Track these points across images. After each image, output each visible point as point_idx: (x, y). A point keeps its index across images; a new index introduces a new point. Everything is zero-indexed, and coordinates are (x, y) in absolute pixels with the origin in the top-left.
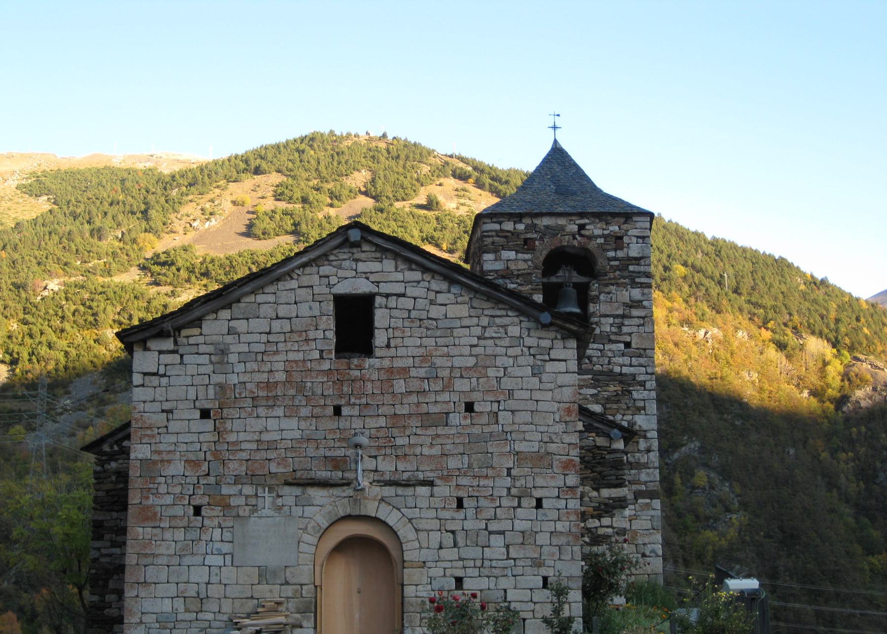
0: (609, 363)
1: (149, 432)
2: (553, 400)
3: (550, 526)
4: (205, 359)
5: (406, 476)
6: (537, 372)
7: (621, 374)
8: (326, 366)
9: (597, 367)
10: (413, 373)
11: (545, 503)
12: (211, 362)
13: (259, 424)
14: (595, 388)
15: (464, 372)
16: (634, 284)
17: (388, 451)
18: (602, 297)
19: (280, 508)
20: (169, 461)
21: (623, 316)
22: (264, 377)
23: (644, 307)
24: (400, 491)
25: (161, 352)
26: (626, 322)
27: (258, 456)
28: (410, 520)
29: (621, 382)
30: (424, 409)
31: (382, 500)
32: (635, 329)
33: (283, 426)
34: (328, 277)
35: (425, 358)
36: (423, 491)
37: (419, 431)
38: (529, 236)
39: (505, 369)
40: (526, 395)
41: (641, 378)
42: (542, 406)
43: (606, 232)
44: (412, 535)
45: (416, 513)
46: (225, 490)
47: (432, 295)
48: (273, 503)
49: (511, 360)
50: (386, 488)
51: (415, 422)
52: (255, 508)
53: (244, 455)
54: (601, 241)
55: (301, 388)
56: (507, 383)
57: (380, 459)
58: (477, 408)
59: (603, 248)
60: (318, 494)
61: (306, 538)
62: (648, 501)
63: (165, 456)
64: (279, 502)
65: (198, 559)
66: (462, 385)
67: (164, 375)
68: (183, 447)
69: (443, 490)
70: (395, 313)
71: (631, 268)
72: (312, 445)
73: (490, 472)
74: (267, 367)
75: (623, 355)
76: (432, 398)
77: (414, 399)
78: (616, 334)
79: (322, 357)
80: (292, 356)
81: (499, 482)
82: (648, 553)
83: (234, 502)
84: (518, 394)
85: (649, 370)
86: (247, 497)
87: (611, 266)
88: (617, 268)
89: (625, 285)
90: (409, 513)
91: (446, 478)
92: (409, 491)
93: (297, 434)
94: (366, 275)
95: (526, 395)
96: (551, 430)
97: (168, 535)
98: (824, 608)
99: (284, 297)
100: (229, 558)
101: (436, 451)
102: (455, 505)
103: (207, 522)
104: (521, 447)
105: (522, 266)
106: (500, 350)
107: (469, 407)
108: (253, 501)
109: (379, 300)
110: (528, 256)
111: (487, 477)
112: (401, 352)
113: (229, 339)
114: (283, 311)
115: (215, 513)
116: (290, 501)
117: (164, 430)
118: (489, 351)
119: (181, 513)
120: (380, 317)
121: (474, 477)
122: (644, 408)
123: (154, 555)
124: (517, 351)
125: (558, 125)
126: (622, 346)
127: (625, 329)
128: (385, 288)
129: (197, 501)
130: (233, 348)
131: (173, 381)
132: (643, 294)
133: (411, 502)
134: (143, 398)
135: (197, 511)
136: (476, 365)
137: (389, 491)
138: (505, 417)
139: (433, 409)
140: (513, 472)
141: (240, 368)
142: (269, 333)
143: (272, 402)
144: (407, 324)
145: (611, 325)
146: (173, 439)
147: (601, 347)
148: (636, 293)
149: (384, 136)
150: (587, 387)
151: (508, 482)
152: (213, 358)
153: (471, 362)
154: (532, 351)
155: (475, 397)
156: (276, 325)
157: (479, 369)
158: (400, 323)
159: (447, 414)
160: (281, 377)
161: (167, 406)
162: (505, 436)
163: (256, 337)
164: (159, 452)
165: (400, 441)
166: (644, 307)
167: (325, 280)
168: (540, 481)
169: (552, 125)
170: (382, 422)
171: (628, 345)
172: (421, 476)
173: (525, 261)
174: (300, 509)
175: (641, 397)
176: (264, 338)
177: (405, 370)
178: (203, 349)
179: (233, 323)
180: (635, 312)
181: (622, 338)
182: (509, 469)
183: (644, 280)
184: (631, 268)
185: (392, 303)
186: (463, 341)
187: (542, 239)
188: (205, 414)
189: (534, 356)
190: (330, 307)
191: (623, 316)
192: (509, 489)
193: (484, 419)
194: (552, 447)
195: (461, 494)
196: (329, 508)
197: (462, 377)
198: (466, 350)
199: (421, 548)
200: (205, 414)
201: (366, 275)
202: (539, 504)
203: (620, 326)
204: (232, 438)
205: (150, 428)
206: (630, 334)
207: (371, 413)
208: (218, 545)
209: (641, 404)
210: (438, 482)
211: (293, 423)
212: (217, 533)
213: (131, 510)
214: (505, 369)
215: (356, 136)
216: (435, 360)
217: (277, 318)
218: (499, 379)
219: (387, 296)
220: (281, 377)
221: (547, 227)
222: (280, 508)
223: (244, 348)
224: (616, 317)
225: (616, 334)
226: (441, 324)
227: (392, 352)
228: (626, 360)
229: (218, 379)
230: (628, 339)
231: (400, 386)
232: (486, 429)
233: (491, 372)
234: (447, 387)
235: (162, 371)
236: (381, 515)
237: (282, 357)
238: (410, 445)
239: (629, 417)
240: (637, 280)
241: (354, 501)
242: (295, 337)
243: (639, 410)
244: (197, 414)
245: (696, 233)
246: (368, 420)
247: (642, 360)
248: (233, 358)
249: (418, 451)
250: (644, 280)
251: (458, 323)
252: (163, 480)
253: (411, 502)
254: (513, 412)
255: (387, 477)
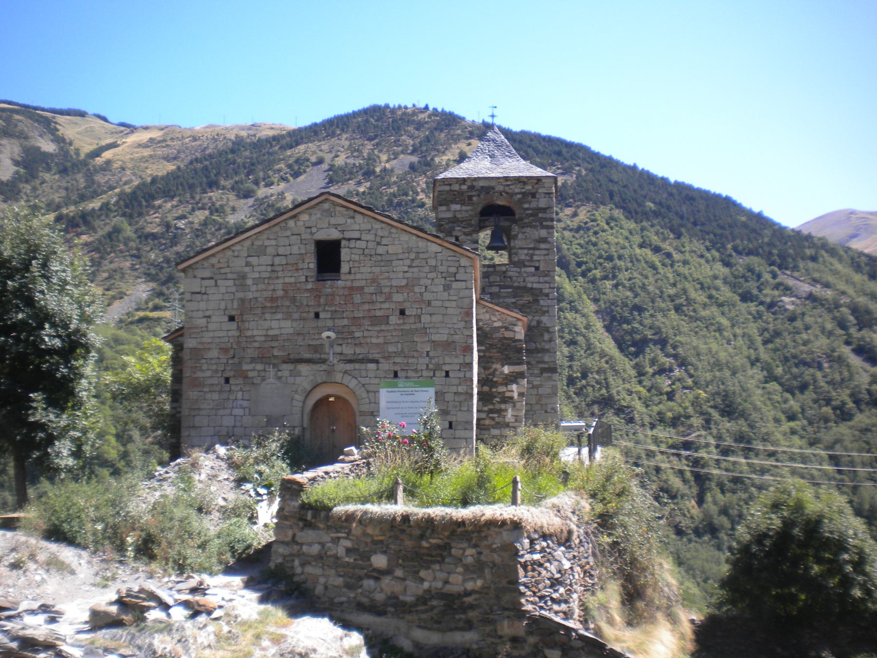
0: (524, 281)
1: (196, 330)
2: (458, 307)
3: (454, 389)
4: (230, 283)
5: (361, 357)
6: (447, 288)
7: (532, 288)
8: (310, 286)
9: (516, 284)
10: (366, 290)
11: (451, 374)
12: (235, 285)
13: (266, 324)
14: (514, 298)
15: (399, 289)
16: (543, 227)
17: (350, 341)
18: (520, 236)
19: (279, 378)
20: (209, 349)
21: (534, 249)
22: (268, 294)
23: (549, 242)
24: (357, 366)
25: (203, 279)
26: (537, 252)
27: (266, 345)
28: (363, 385)
29: (532, 294)
30: (373, 313)
31: (346, 372)
32: (542, 258)
33: (282, 326)
34: (310, 228)
35: (374, 280)
36: (372, 366)
37: (370, 328)
38: (470, 194)
39: (426, 287)
40: (439, 303)
41: (546, 291)
42: (450, 311)
43: (523, 190)
44: (364, 395)
45: (367, 381)
46: (245, 367)
47: (378, 239)
48: (276, 375)
49: (430, 281)
50: (348, 365)
51: (367, 322)
52: (264, 379)
53: (256, 345)
54: (519, 196)
55: (293, 300)
56: (427, 296)
57: (344, 346)
58: (407, 313)
59: (521, 202)
60: (304, 368)
61: (297, 397)
62: (549, 375)
63: (207, 346)
64: (280, 374)
65: (228, 411)
66: (398, 297)
67: (205, 294)
68: (217, 340)
69: (385, 366)
70: (354, 251)
71: (540, 215)
72: (300, 338)
73: (415, 354)
74: (272, 287)
75: (534, 275)
76: (378, 306)
77: (366, 307)
78: (528, 261)
79: (307, 281)
80: (287, 280)
81: (421, 361)
82: (549, 410)
83: (251, 374)
84: (434, 303)
85: (552, 286)
86: (259, 371)
87: (527, 214)
88: (531, 215)
89: (535, 227)
90: (363, 381)
91: (387, 358)
92: (363, 366)
93: (291, 331)
94: (336, 226)
95: (439, 303)
96: (455, 326)
97: (208, 396)
98: (756, 461)
99: (283, 241)
100: (247, 411)
101: (381, 340)
102: (392, 376)
103: (233, 388)
104: (435, 338)
105: (464, 214)
106: (422, 275)
107: (402, 312)
108: (263, 374)
109: (343, 243)
110: (469, 208)
111: (413, 357)
112: (359, 276)
113: (247, 269)
114: (281, 251)
115: (237, 382)
116: (287, 373)
117: (205, 329)
118: (415, 275)
119: (216, 382)
120: (345, 254)
121: (405, 357)
122: (548, 312)
123: (199, 409)
124: (433, 275)
125: (495, 114)
126: (533, 269)
127: (535, 258)
128: (348, 235)
129: (227, 375)
130: (249, 275)
131: (210, 297)
132: (549, 233)
133: (364, 373)
134: (191, 309)
135: (227, 380)
136: (407, 284)
137: (349, 367)
138: (425, 319)
139: (378, 313)
140: (431, 354)
141: (254, 288)
142: (272, 265)
143: (275, 310)
144: (362, 258)
145: (526, 255)
146: (211, 334)
147: (518, 270)
148: (543, 233)
149: (427, 108)
150: (509, 297)
151: (427, 360)
152: (237, 282)
153: (404, 282)
154: (444, 275)
155: (406, 305)
156: (277, 260)
157: (409, 286)
158: (357, 258)
159: (388, 317)
160: (280, 293)
161: (208, 313)
162: (424, 331)
163: (263, 268)
164: (202, 343)
165: (357, 334)
166: (549, 242)
167: (308, 230)
168: (448, 360)
169: (490, 114)
170: (345, 322)
171: (537, 268)
172: (371, 357)
173: (467, 211)
174: (292, 378)
175: (545, 304)
176: (269, 269)
177: (362, 288)
178: (229, 276)
179: (249, 259)
180: (542, 246)
181: (533, 264)
182: (428, 352)
183: (549, 223)
184: (540, 215)
185: (352, 244)
186: (398, 269)
187: (479, 196)
188: (232, 319)
189: (445, 278)
190: (312, 248)
191: (534, 249)
192: (427, 365)
193: (412, 320)
194: (456, 338)
195: (397, 368)
196: (311, 378)
197: (398, 292)
198: (401, 275)
199: (370, 403)
200: (232, 319)
201: (336, 226)
202: (447, 374)
203: (532, 255)
204: (249, 333)
205: (197, 328)
206: (539, 261)
207: (339, 316)
208: (240, 402)
209: (545, 309)
210: (381, 360)
211: (288, 323)
212: (240, 395)
213: (185, 381)
214: (426, 287)
215: (406, 108)
216: (380, 281)
217: (278, 255)
218: (421, 294)
219: (349, 240)
220: (280, 293)
221: (482, 187)
222: (279, 378)
223: (257, 275)
224: (530, 249)
225: (528, 261)
226: (384, 258)
227: (352, 277)
228: (536, 279)
229: (240, 295)
230: (537, 265)
231: (357, 298)
232: (413, 327)
233: (417, 289)
234: (389, 298)
235: (203, 291)
236: (345, 381)
237: (281, 281)
238: (363, 337)
239: (537, 318)
240: (544, 223)
241: (329, 373)
242: (290, 268)
243: (544, 313)
244: (226, 319)
245: (663, 179)
246: (336, 321)
247: (547, 279)
248: (249, 282)
249: (369, 340)
250: (549, 223)
251: (394, 257)
252: (204, 361)
253: (364, 373)
254: (431, 315)
255: (349, 358)
